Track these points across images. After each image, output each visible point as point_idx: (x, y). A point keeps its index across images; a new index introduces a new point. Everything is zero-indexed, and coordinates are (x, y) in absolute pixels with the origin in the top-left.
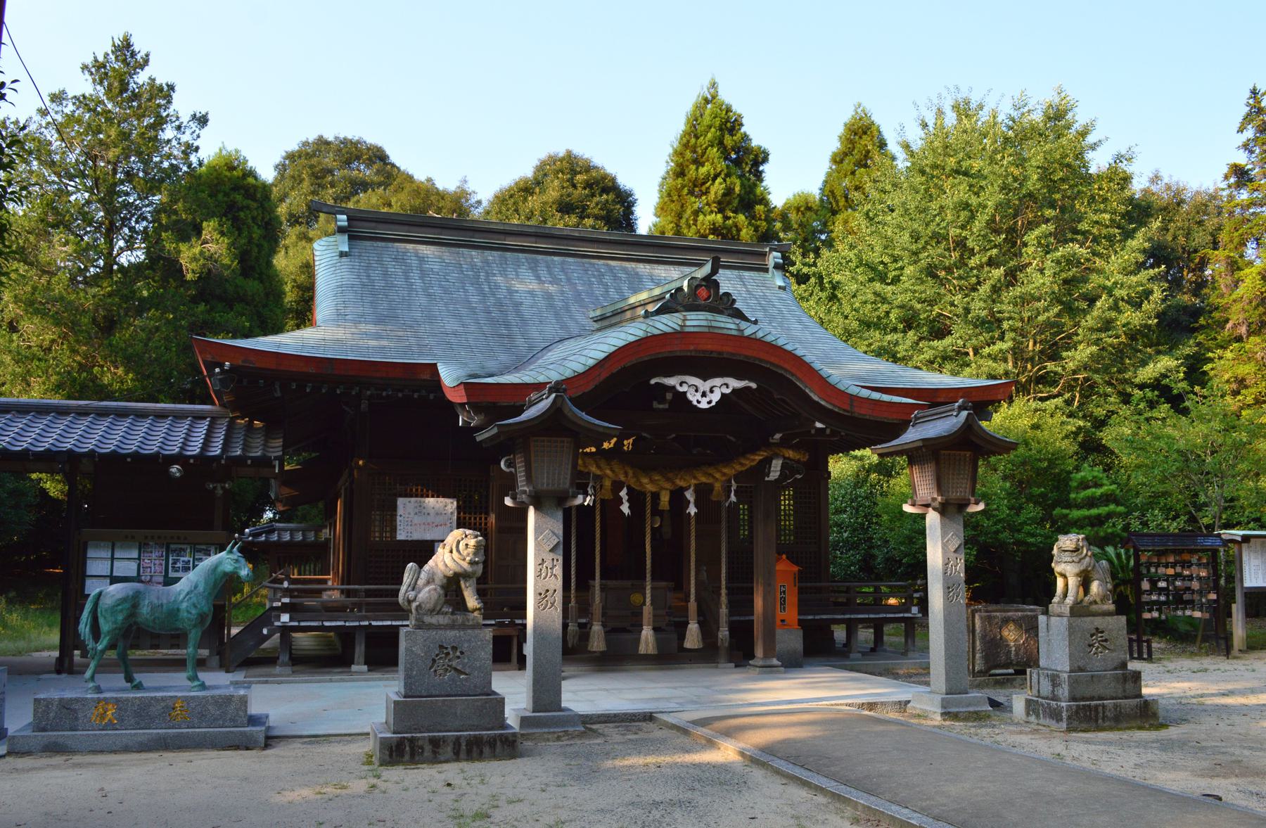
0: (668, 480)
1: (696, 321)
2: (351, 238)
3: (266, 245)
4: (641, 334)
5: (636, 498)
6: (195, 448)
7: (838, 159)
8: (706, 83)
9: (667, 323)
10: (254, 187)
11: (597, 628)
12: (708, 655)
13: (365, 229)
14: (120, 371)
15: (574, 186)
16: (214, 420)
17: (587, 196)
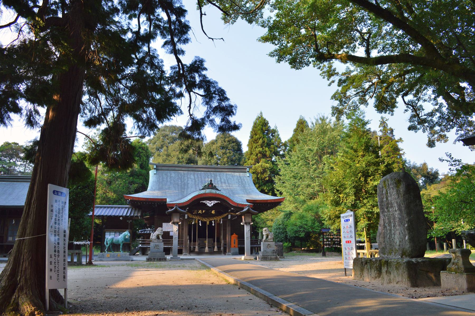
0: (208, 219)
1: (208, 191)
2: (157, 170)
3: (147, 161)
4: (198, 194)
6: (124, 214)
7: (295, 131)
8: (259, 113)
9: (203, 192)
10: (144, 147)
11: (197, 247)
12: (219, 252)
13: (160, 168)
14: (113, 194)
15: (225, 142)
16: (129, 208)
17: (228, 144)
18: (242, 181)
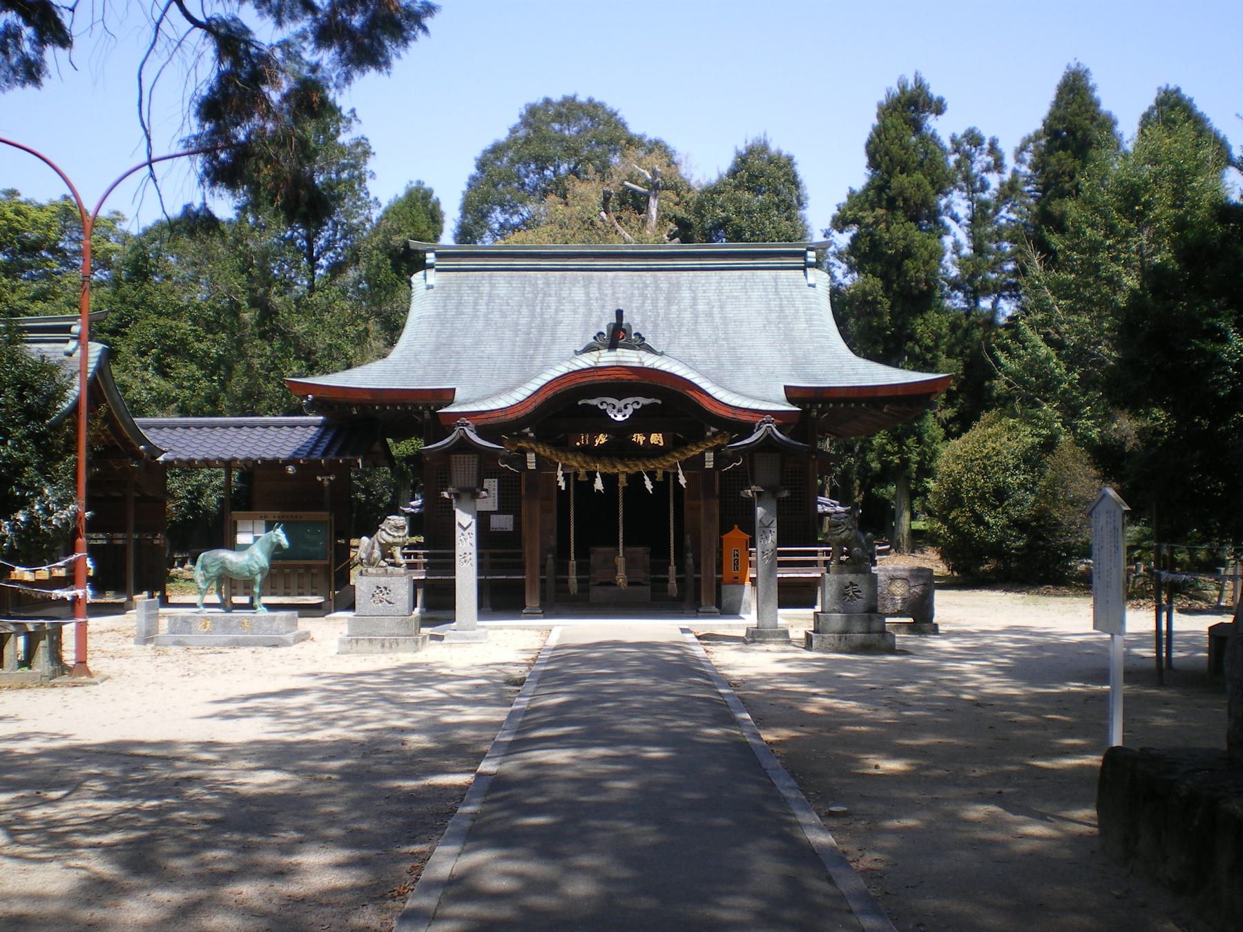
1: (606, 358)
5: (609, 480)
18: (781, 306)
